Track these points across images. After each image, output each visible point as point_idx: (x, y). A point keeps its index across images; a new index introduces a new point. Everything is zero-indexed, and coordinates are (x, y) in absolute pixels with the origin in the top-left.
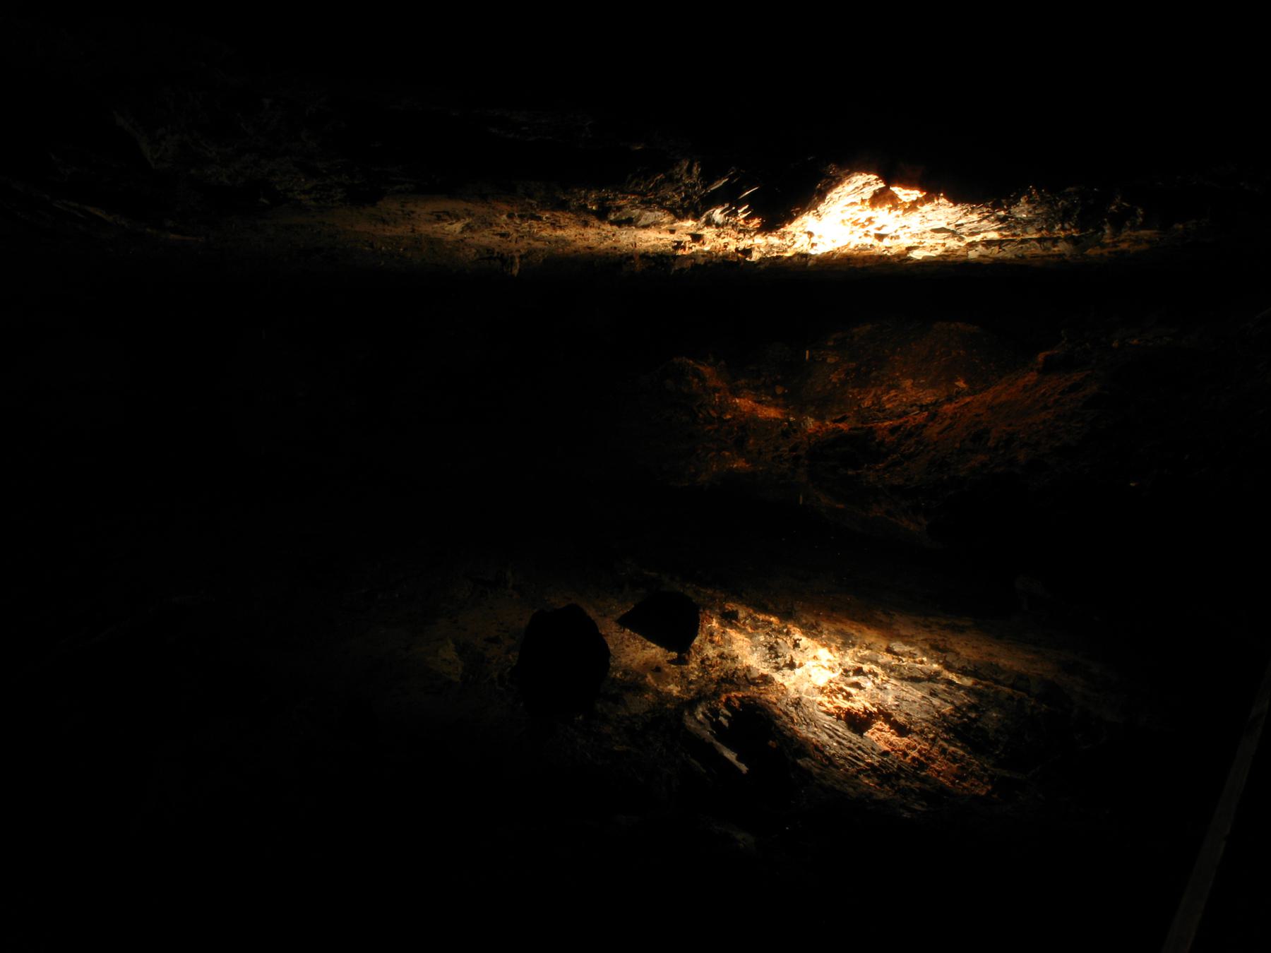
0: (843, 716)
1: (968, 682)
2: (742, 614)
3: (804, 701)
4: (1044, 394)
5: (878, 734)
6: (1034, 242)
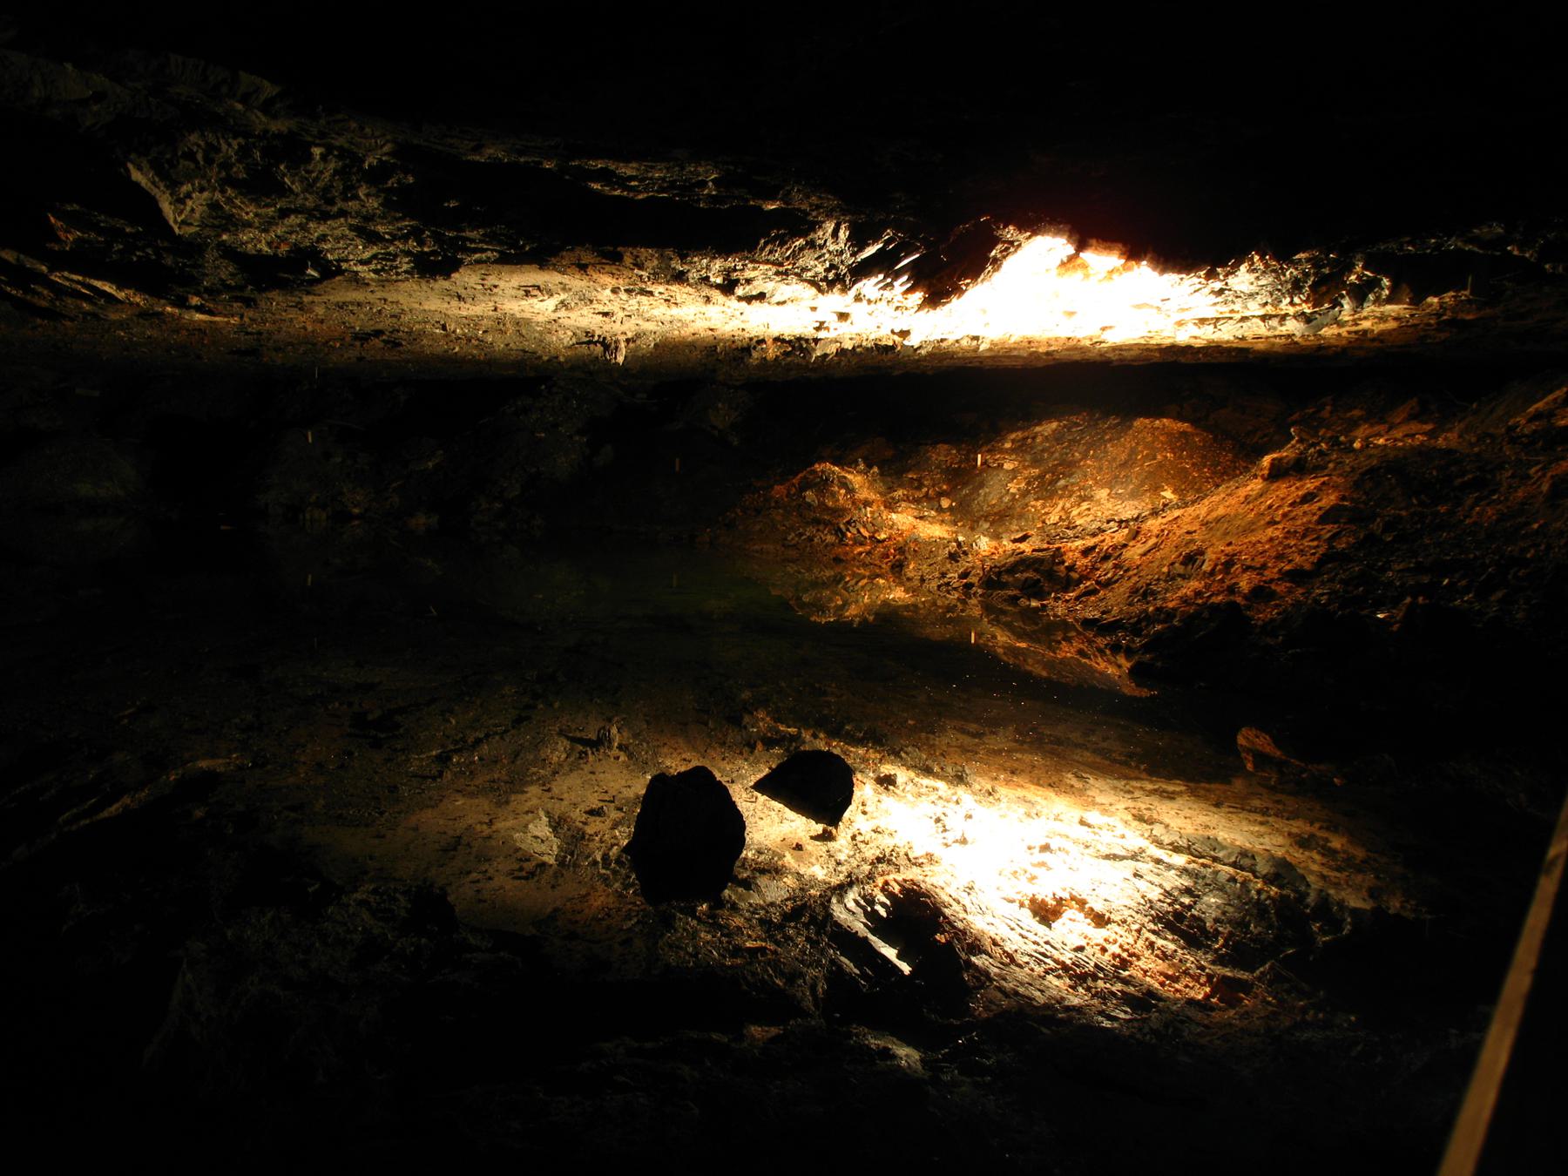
1: (1180, 860)
4: (1270, 507)
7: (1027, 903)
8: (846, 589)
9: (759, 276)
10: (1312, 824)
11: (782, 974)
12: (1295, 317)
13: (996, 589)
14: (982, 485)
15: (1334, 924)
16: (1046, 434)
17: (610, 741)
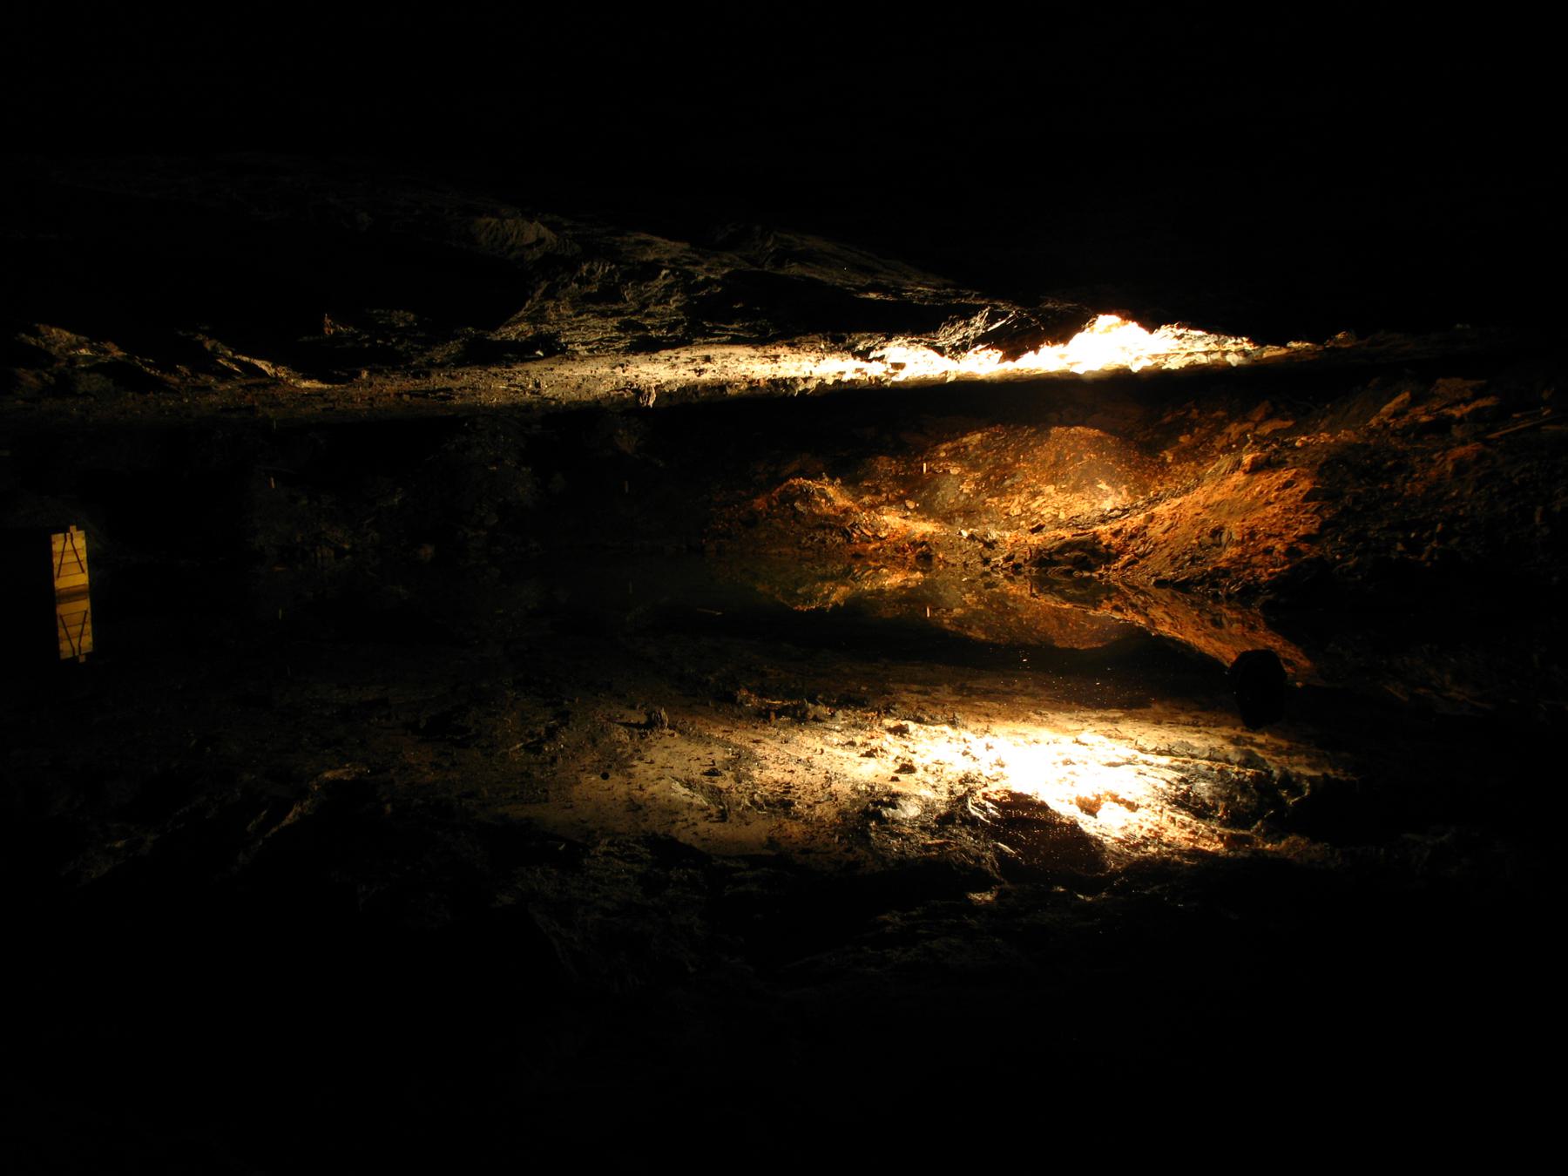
1: (1166, 760)
4: (1261, 492)
7: (1074, 801)
8: (853, 579)
10: (1235, 729)
11: (971, 857)
12: (1236, 352)
13: (1050, 566)
14: (937, 488)
15: (1295, 789)
16: (974, 443)
17: (662, 722)
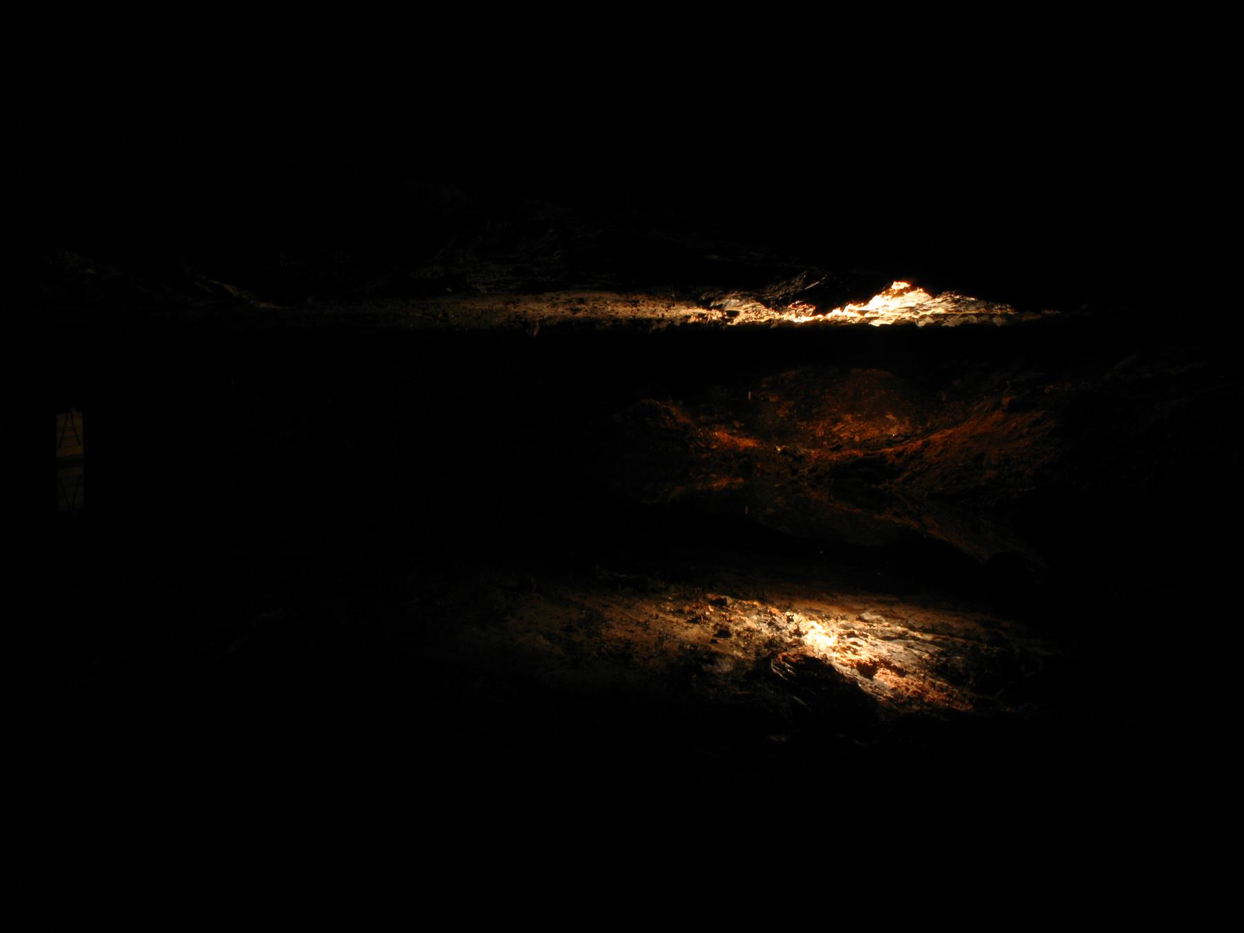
0: (855, 666)
1: (929, 637)
2: (730, 601)
3: (828, 657)
5: (884, 676)
6: (972, 316)
9: (907, 319)
